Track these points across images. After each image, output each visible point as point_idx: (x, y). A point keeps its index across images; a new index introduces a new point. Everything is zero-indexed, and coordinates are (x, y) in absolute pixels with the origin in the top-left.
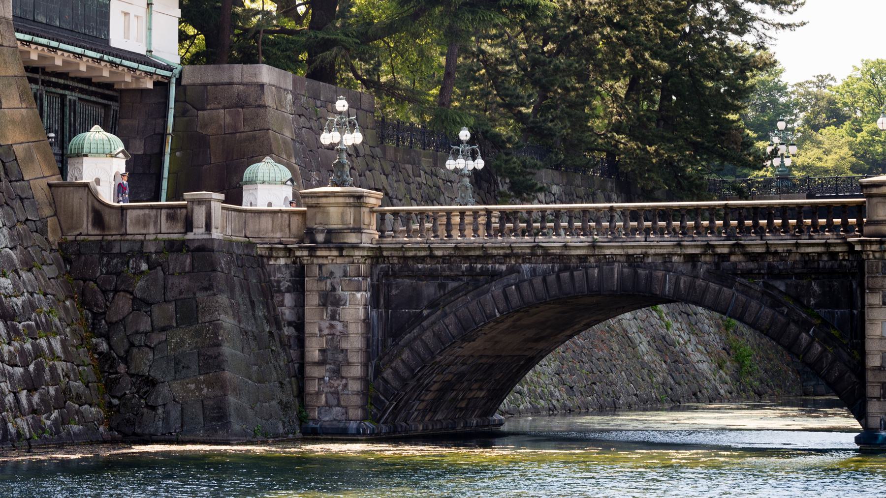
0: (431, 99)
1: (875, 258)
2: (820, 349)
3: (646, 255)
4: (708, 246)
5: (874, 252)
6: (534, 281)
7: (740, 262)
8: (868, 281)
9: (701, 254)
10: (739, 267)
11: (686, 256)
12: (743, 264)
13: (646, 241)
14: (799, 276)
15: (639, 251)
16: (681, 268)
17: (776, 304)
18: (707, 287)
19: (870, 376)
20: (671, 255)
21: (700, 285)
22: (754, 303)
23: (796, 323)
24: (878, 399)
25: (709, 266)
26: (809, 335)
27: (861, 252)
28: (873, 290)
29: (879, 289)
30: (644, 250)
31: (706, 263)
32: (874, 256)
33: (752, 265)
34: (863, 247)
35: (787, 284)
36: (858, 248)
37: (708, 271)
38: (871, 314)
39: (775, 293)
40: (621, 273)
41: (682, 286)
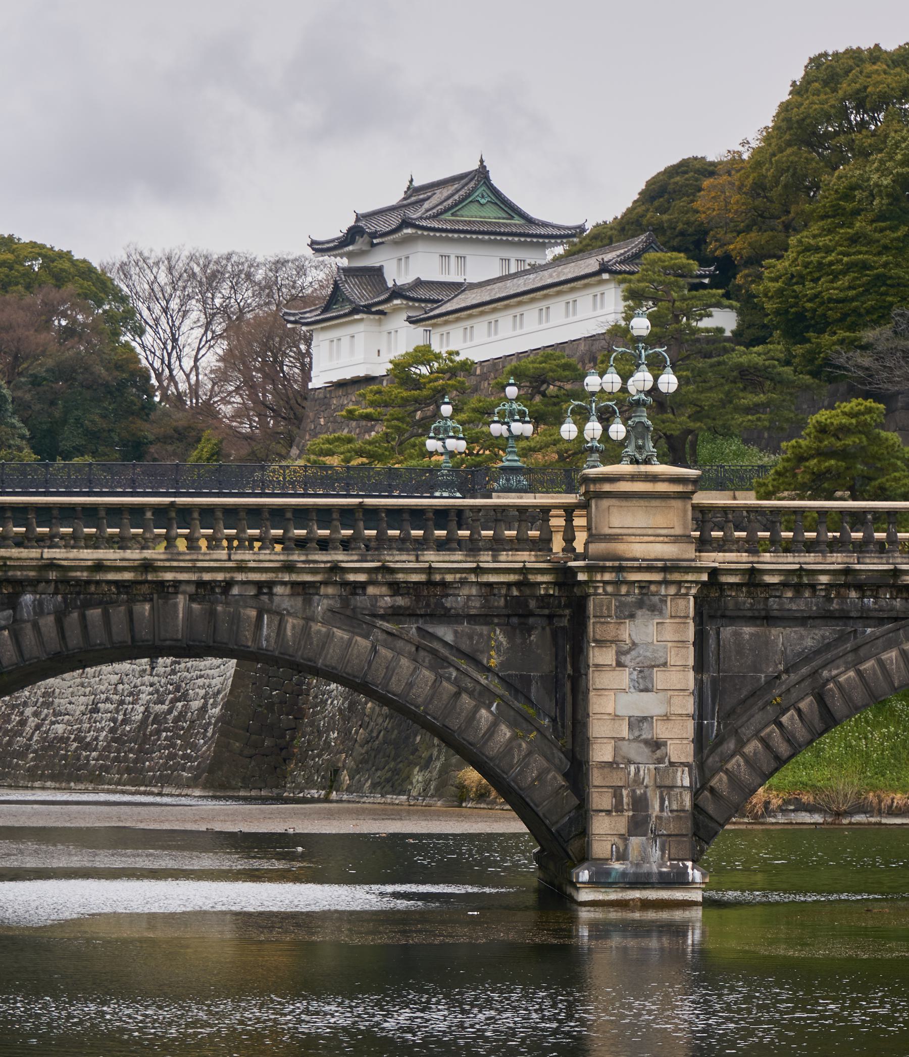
0: (56, 323)
1: (606, 593)
2: (508, 734)
3: (229, 584)
4: (335, 568)
5: (606, 583)
6: (42, 622)
7: (382, 596)
8: (594, 629)
9: (321, 583)
10: (381, 603)
11: (294, 584)
12: (387, 599)
13: (417, 561)
14: (472, 619)
15: (220, 577)
16: (286, 604)
17: (439, 662)
18: (329, 636)
19: (596, 778)
20: (270, 584)
21: (319, 632)
22: (404, 662)
23: (471, 694)
24: (608, 812)
25: (331, 602)
26: (491, 712)
27: (586, 582)
28: (601, 643)
29: (612, 642)
30: (228, 576)
31: (327, 596)
32: (604, 590)
33: (400, 601)
34: (590, 576)
35: (456, 632)
36: (582, 577)
37: (331, 610)
38: (597, 680)
39: (436, 645)
40: (189, 611)
41: (289, 633)
